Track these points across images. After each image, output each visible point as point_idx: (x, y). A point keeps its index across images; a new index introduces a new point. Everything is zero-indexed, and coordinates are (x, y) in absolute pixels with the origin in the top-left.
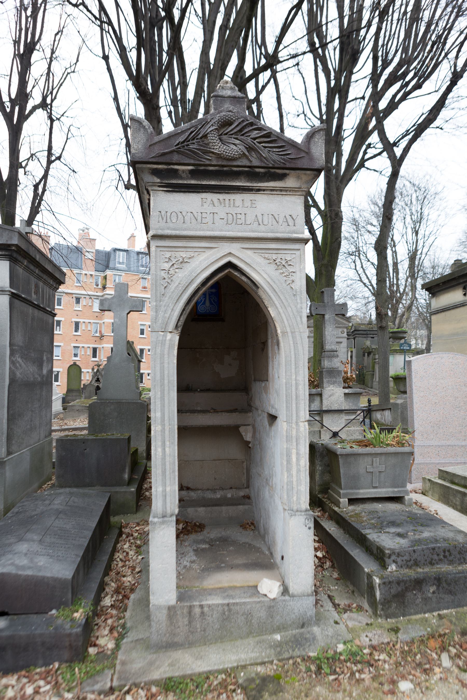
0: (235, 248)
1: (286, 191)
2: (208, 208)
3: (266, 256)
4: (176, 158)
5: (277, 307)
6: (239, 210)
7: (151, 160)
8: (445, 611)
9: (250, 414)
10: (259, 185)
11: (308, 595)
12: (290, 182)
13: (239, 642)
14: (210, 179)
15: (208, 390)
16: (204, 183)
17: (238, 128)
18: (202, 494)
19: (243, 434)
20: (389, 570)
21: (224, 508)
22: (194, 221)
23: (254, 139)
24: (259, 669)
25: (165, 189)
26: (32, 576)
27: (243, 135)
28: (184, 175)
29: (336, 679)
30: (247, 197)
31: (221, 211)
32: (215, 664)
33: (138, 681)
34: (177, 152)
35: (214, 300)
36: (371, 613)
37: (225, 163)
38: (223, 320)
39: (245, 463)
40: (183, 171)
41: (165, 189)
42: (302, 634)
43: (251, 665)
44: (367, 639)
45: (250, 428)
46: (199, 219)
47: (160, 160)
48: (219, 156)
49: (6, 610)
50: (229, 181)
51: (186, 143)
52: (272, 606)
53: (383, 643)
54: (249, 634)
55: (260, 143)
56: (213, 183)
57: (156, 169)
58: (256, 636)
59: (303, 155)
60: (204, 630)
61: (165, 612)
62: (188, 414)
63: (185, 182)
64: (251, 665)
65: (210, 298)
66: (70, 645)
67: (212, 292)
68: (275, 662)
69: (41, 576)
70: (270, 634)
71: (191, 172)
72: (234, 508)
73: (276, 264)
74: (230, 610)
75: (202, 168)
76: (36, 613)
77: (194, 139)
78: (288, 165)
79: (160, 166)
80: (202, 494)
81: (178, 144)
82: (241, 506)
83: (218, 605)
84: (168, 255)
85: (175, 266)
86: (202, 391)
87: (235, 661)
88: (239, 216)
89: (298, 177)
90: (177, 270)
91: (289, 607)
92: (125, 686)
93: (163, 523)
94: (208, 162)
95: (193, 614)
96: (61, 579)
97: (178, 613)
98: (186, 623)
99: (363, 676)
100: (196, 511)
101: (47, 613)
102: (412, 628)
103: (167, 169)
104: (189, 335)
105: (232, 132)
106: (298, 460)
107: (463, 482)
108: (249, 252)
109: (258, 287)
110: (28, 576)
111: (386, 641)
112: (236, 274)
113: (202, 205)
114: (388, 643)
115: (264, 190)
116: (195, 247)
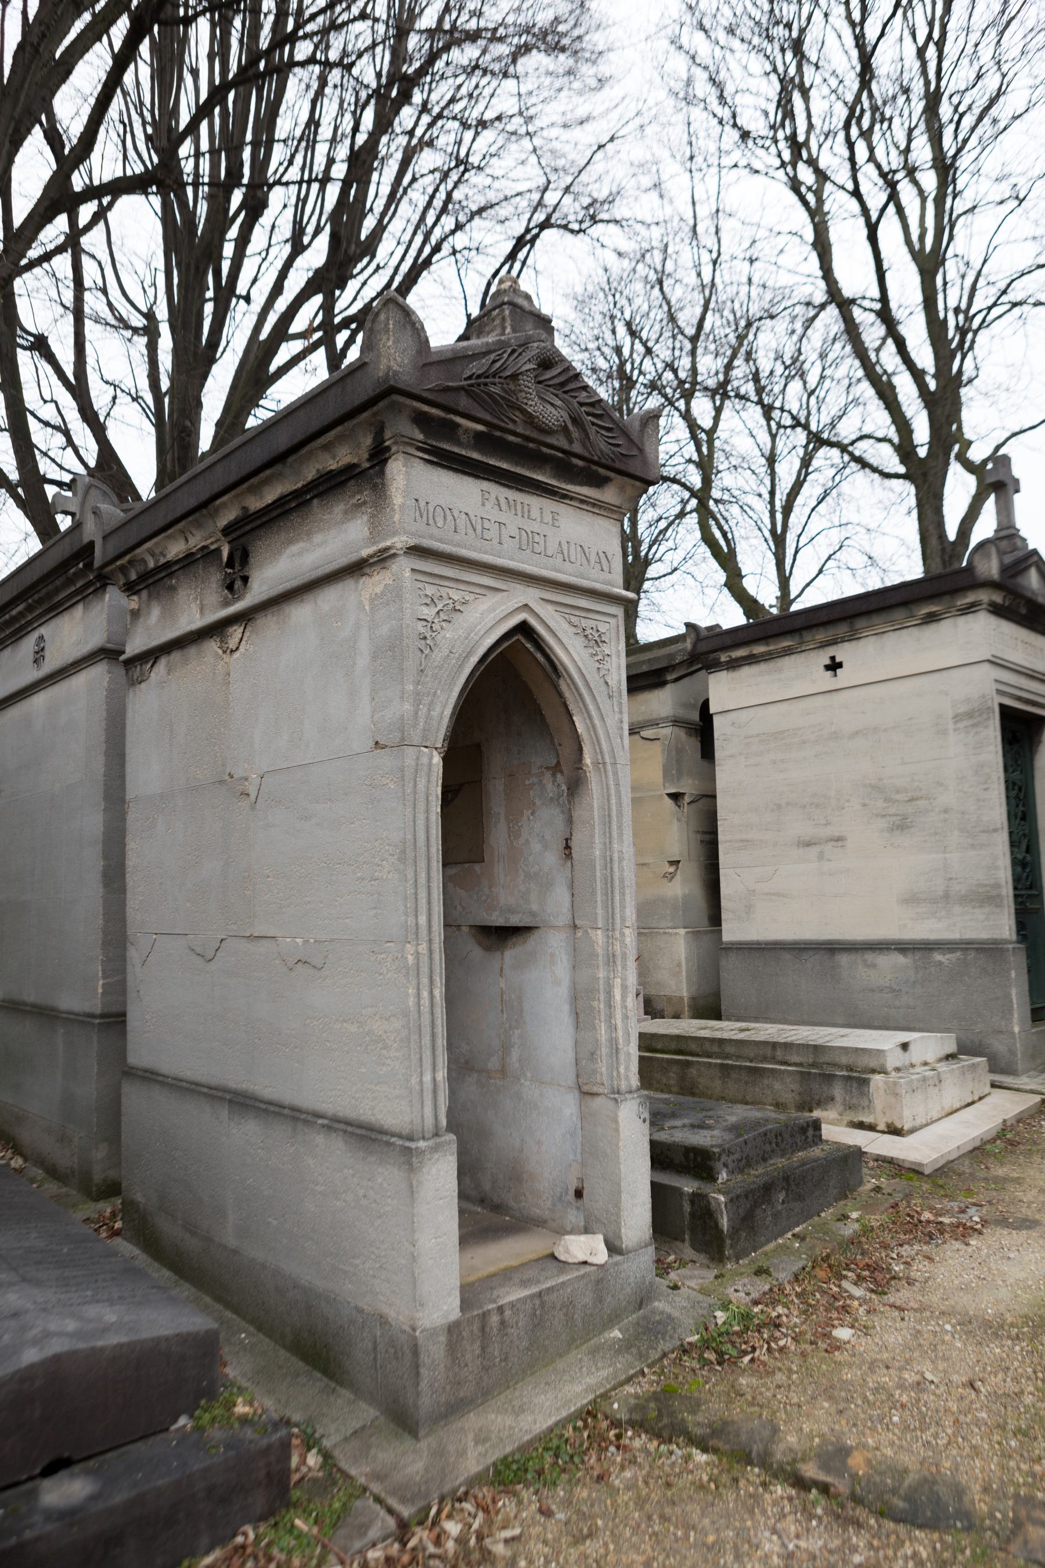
0: (530, 595)
1: (600, 507)
2: (491, 512)
3: (573, 619)
4: (464, 402)
5: (590, 717)
6: (535, 527)
7: (425, 394)
8: (797, 1229)
10: (569, 487)
11: (646, 1246)
12: (609, 495)
13: (560, 1364)
14: (501, 459)
16: (492, 462)
17: (562, 379)
20: (720, 1181)
22: (470, 531)
23: (581, 404)
24: (630, 1389)
25: (426, 457)
26: (129, 1344)
27: (566, 392)
28: (464, 438)
29: (752, 1360)
30: (548, 505)
31: (513, 523)
32: (558, 1409)
33: (447, 1488)
34: (467, 391)
36: (706, 1261)
37: (534, 434)
40: (467, 430)
41: (426, 457)
42: (645, 1318)
43: (614, 1388)
44: (742, 1294)
46: (479, 527)
47: (440, 399)
48: (530, 420)
49: (66, 1455)
50: (528, 469)
51: (482, 380)
52: (599, 1278)
53: (765, 1293)
54: (572, 1343)
55: (588, 414)
56: (505, 466)
57: (425, 413)
58: (582, 1344)
59: (635, 452)
60: (506, 1359)
61: (443, 1339)
63: (464, 453)
64: (614, 1388)
66: (268, 1474)
68: (646, 1370)
69: (153, 1339)
70: (600, 1333)
71: (478, 435)
73: (586, 636)
74: (543, 1305)
75: (498, 434)
76: (141, 1438)
77: (494, 376)
78: (618, 465)
79: (434, 411)
81: (470, 378)
83: (523, 1301)
84: (430, 590)
85: (443, 616)
87: (586, 1391)
88: (537, 538)
89: (622, 489)
90: (444, 624)
91: (623, 1275)
92: (430, 1508)
93: (435, 1149)
94: (511, 426)
95: (488, 1330)
96: (198, 1333)
97: (464, 1334)
98: (478, 1352)
99: (782, 1343)
101: (167, 1429)
102: (310, 1443)
103: (444, 419)
105: (551, 383)
106: (624, 997)
107: (673, 1046)
108: (550, 608)
109: (559, 676)
110: (121, 1346)
111: (767, 1287)
112: (528, 646)
113: (483, 505)
114: (771, 1290)
115: (572, 498)
116: (473, 584)
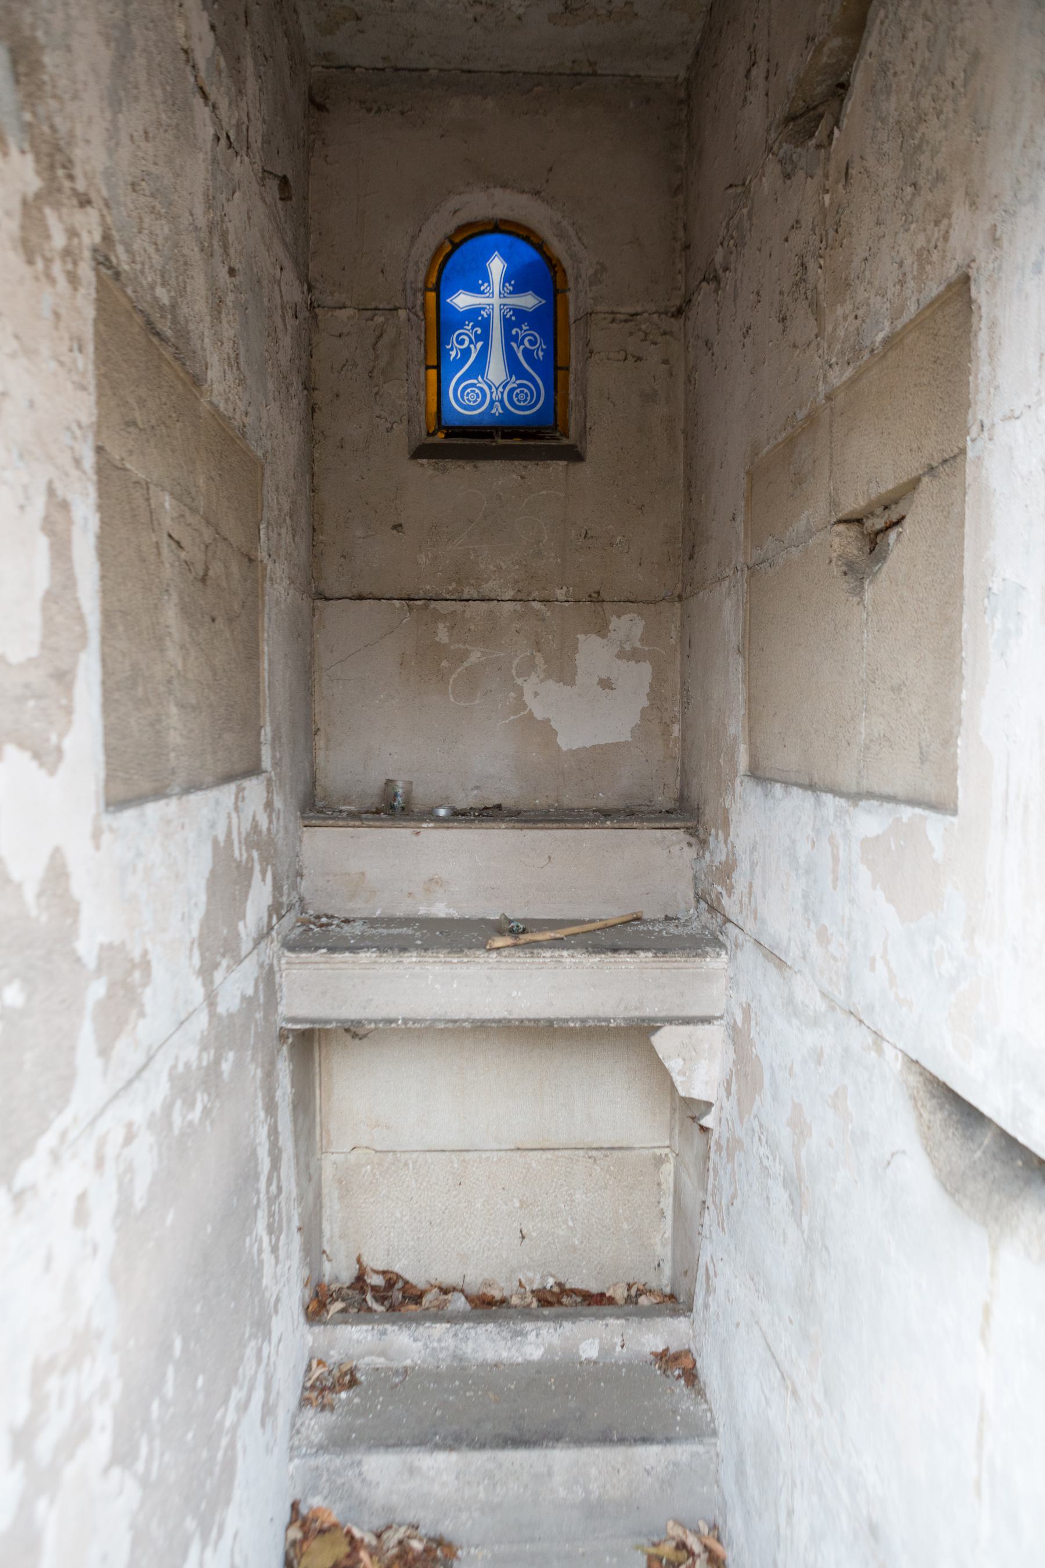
9: (716, 963)
15: (489, 814)
18: (450, 1342)
19: (674, 1065)
21: (561, 1459)
35: (527, 353)
38: (574, 455)
39: (669, 1168)
45: (715, 1033)
62: (364, 957)
65: (508, 338)
67: (518, 312)
72: (617, 1455)
80: (450, 1342)
82: (654, 1450)
86: (460, 816)
100: (412, 1471)
104: (397, 527)
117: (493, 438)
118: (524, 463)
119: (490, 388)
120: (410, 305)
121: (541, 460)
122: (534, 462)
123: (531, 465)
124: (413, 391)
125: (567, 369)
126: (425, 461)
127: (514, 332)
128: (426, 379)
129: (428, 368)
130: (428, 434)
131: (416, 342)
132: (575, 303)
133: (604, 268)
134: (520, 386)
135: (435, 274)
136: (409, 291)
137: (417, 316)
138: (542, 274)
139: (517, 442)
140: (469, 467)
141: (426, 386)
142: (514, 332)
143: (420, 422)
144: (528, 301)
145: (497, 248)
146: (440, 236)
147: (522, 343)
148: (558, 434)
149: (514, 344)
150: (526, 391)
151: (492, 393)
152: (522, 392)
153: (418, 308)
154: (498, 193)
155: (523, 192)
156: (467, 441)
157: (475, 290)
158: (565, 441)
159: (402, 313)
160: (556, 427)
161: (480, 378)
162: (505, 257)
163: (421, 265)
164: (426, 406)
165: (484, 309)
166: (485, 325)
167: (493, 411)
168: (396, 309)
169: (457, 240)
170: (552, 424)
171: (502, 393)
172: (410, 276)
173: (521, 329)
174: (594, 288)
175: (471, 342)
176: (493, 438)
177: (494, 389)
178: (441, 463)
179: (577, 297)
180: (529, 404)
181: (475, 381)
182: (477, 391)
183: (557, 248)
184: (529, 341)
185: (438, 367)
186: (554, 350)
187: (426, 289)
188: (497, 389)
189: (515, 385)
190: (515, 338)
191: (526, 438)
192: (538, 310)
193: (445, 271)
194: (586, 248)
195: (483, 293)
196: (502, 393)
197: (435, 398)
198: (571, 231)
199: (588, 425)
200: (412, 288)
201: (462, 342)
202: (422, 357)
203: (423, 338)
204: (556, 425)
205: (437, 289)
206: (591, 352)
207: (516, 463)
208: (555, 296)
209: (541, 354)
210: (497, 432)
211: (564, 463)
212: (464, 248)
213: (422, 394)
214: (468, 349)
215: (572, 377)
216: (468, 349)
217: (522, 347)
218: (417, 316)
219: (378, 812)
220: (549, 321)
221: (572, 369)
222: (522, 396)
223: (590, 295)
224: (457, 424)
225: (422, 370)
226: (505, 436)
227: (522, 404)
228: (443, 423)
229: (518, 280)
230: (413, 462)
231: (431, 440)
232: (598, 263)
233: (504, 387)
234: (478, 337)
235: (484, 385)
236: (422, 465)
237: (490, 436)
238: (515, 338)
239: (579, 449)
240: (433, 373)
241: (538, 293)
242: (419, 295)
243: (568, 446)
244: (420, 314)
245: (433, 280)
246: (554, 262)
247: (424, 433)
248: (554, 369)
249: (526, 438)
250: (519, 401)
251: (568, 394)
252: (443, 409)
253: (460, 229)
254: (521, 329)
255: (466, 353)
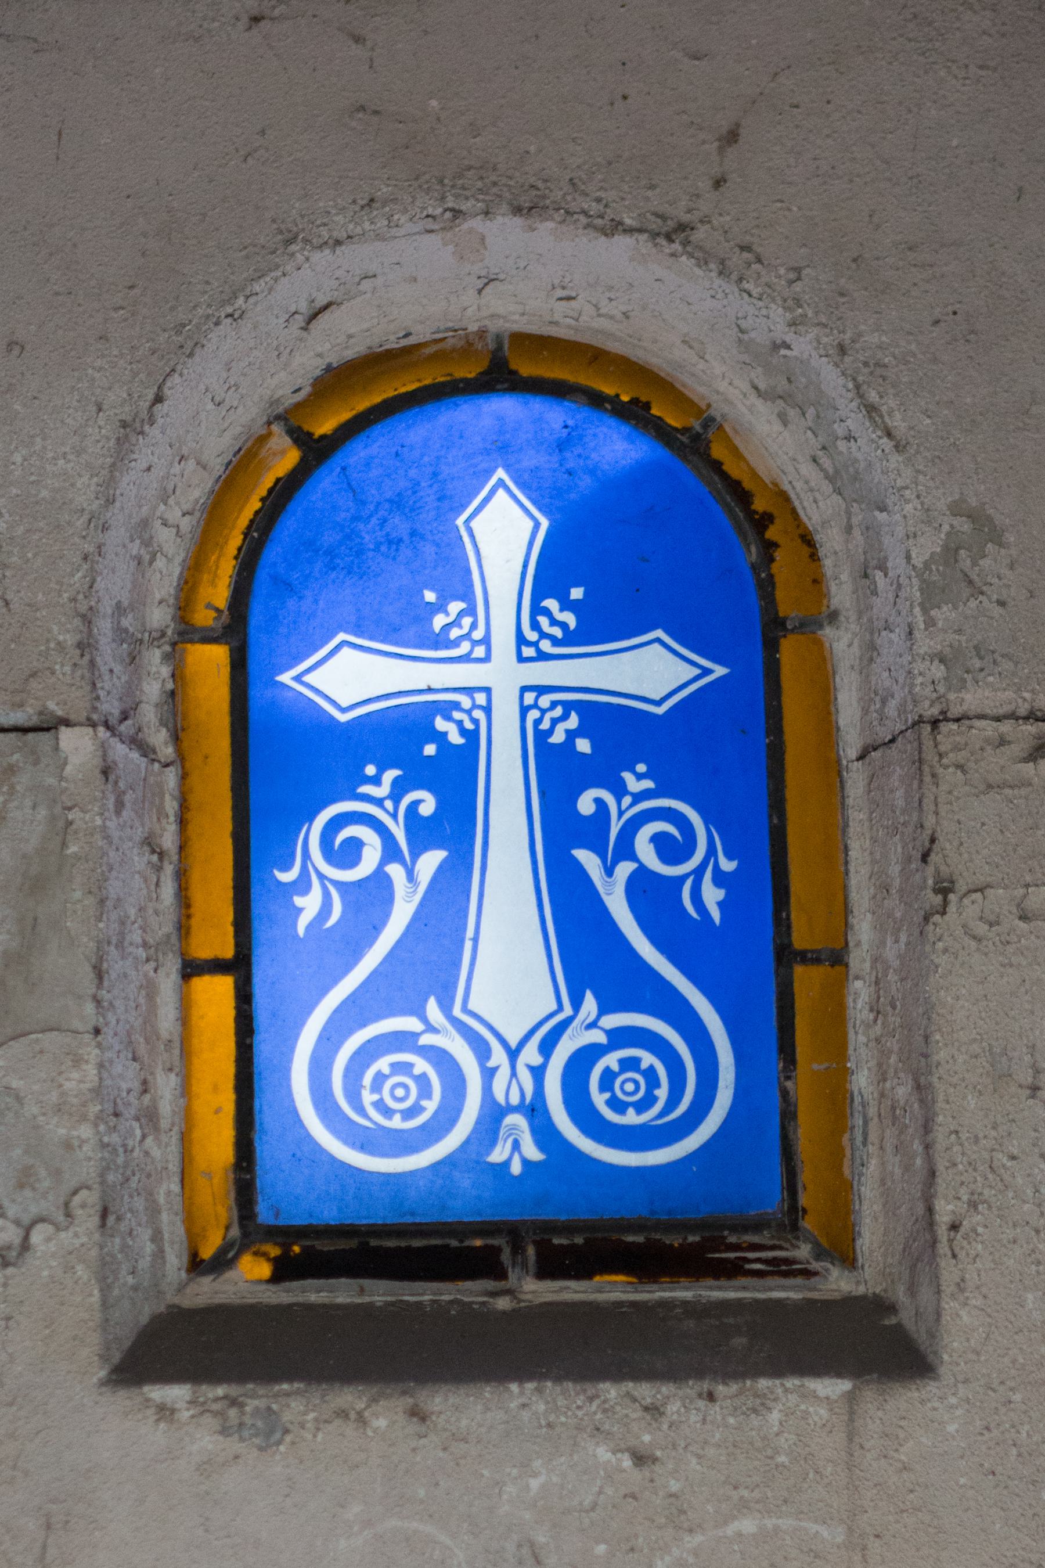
35: (650, 895)
38: (882, 1347)
65: (561, 834)
67: (616, 730)
117: (499, 1273)
118: (645, 1391)
119: (482, 1051)
120: (111, 707)
121: (728, 1376)
122: (692, 1388)
123: (678, 1400)
124: (126, 1076)
125: (837, 958)
126: (177, 1393)
127: (586, 805)
128: (185, 1019)
129: (191, 969)
130: (196, 1265)
131: (141, 860)
132: (866, 668)
133: (986, 529)
134: (619, 1037)
135: (226, 568)
136: (108, 653)
137: (146, 750)
138: (687, 530)
139: (612, 1289)
140: (385, 1415)
141: (186, 1052)
142: (586, 805)
143: (154, 1210)
144: (650, 671)
145: (502, 450)
146: (247, 414)
147: (626, 850)
148: (803, 1251)
149: (588, 859)
150: (648, 1059)
151: (489, 1074)
152: (630, 1064)
153: (149, 715)
154: (504, 235)
155: (615, 228)
156: (380, 1292)
157: (404, 628)
158: (837, 1283)
159: (77, 745)
160: (791, 1218)
161: (433, 1009)
162: (537, 489)
163: (164, 536)
164: (185, 1139)
165: (447, 709)
166: (455, 775)
167: (498, 1155)
168: (49, 726)
169: (325, 426)
170: (773, 1202)
171: (538, 1073)
172: (115, 585)
173: (619, 790)
174: (943, 614)
175: (391, 852)
176: (499, 1273)
177: (499, 1057)
178: (257, 1398)
179: (871, 649)
180: (666, 1119)
181: (410, 1024)
182: (421, 1065)
183: (773, 446)
184: (659, 841)
185: (239, 966)
186: (771, 869)
187: (187, 633)
188: (513, 1054)
189: (598, 1037)
190: (593, 831)
191: (666, 1273)
192: (692, 708)
193: (273, 554)
194: (899, 448)
195: (441, 641)
196: (538, 1073)
197: (227, 1100)
198: (831, 379)
199: (945, 1210)
200: (121, 634)
201: (352, 852)
202: (165, 926)
203: (169, 840)
204: (794, 1211)
205: (234, 629)
206: (944, 890)
207: (611, 1391)
208: (771, 646)
209: (712, 895)
210: (517, 1248)
211: (832, 1388)
212: (357, 453)
213: (166, 1085)
214: (380, 880)
215: (860, 994)
216: (380, 880)
217: (625, 869)
218: (146, 750)
219: (104, 760)
220: (749, 753)
221: (859, 960)
222: (627, 1085)
223: (925, 644)
224: (329, 1215)
225: (168, 980)
226: (551, 1267)
227: (631, 1118)
228: (264, 1214)
229: (596, 578)
230: (123, 1398)
231: (207, 1291)
232: (957, 509)
233: (547, 1047)
234: (423, 833)
235: (444, 1028)
236: (165, 1412)
237: (482, 1265)
238: (593, 831)
239: (906, 1317)
240: (216, 993)
241: (692, 635)
242: (154, 658)
243: (849, 1302)
244: (159, 738)
245: (218, 592)
246: (759, 505)
247: (175, 1261)
248: (777, 962)
249: (666, 1273)
250: (615, 1104)
251: (843, 1073)
252: (266, 1150)
253: (335, 380)
254: (619, 790)
255: (374, 895)
